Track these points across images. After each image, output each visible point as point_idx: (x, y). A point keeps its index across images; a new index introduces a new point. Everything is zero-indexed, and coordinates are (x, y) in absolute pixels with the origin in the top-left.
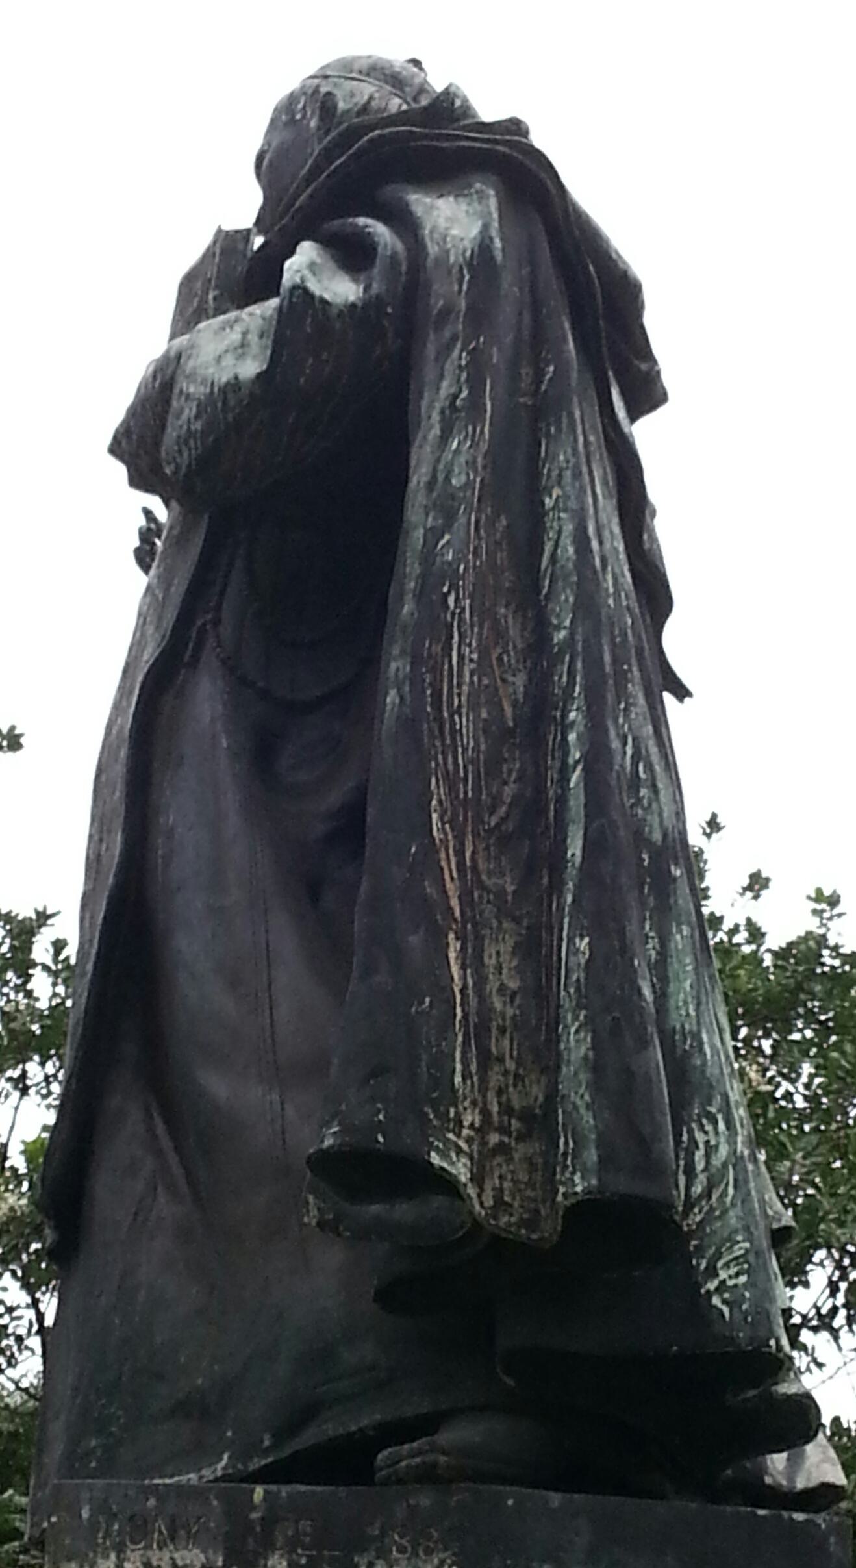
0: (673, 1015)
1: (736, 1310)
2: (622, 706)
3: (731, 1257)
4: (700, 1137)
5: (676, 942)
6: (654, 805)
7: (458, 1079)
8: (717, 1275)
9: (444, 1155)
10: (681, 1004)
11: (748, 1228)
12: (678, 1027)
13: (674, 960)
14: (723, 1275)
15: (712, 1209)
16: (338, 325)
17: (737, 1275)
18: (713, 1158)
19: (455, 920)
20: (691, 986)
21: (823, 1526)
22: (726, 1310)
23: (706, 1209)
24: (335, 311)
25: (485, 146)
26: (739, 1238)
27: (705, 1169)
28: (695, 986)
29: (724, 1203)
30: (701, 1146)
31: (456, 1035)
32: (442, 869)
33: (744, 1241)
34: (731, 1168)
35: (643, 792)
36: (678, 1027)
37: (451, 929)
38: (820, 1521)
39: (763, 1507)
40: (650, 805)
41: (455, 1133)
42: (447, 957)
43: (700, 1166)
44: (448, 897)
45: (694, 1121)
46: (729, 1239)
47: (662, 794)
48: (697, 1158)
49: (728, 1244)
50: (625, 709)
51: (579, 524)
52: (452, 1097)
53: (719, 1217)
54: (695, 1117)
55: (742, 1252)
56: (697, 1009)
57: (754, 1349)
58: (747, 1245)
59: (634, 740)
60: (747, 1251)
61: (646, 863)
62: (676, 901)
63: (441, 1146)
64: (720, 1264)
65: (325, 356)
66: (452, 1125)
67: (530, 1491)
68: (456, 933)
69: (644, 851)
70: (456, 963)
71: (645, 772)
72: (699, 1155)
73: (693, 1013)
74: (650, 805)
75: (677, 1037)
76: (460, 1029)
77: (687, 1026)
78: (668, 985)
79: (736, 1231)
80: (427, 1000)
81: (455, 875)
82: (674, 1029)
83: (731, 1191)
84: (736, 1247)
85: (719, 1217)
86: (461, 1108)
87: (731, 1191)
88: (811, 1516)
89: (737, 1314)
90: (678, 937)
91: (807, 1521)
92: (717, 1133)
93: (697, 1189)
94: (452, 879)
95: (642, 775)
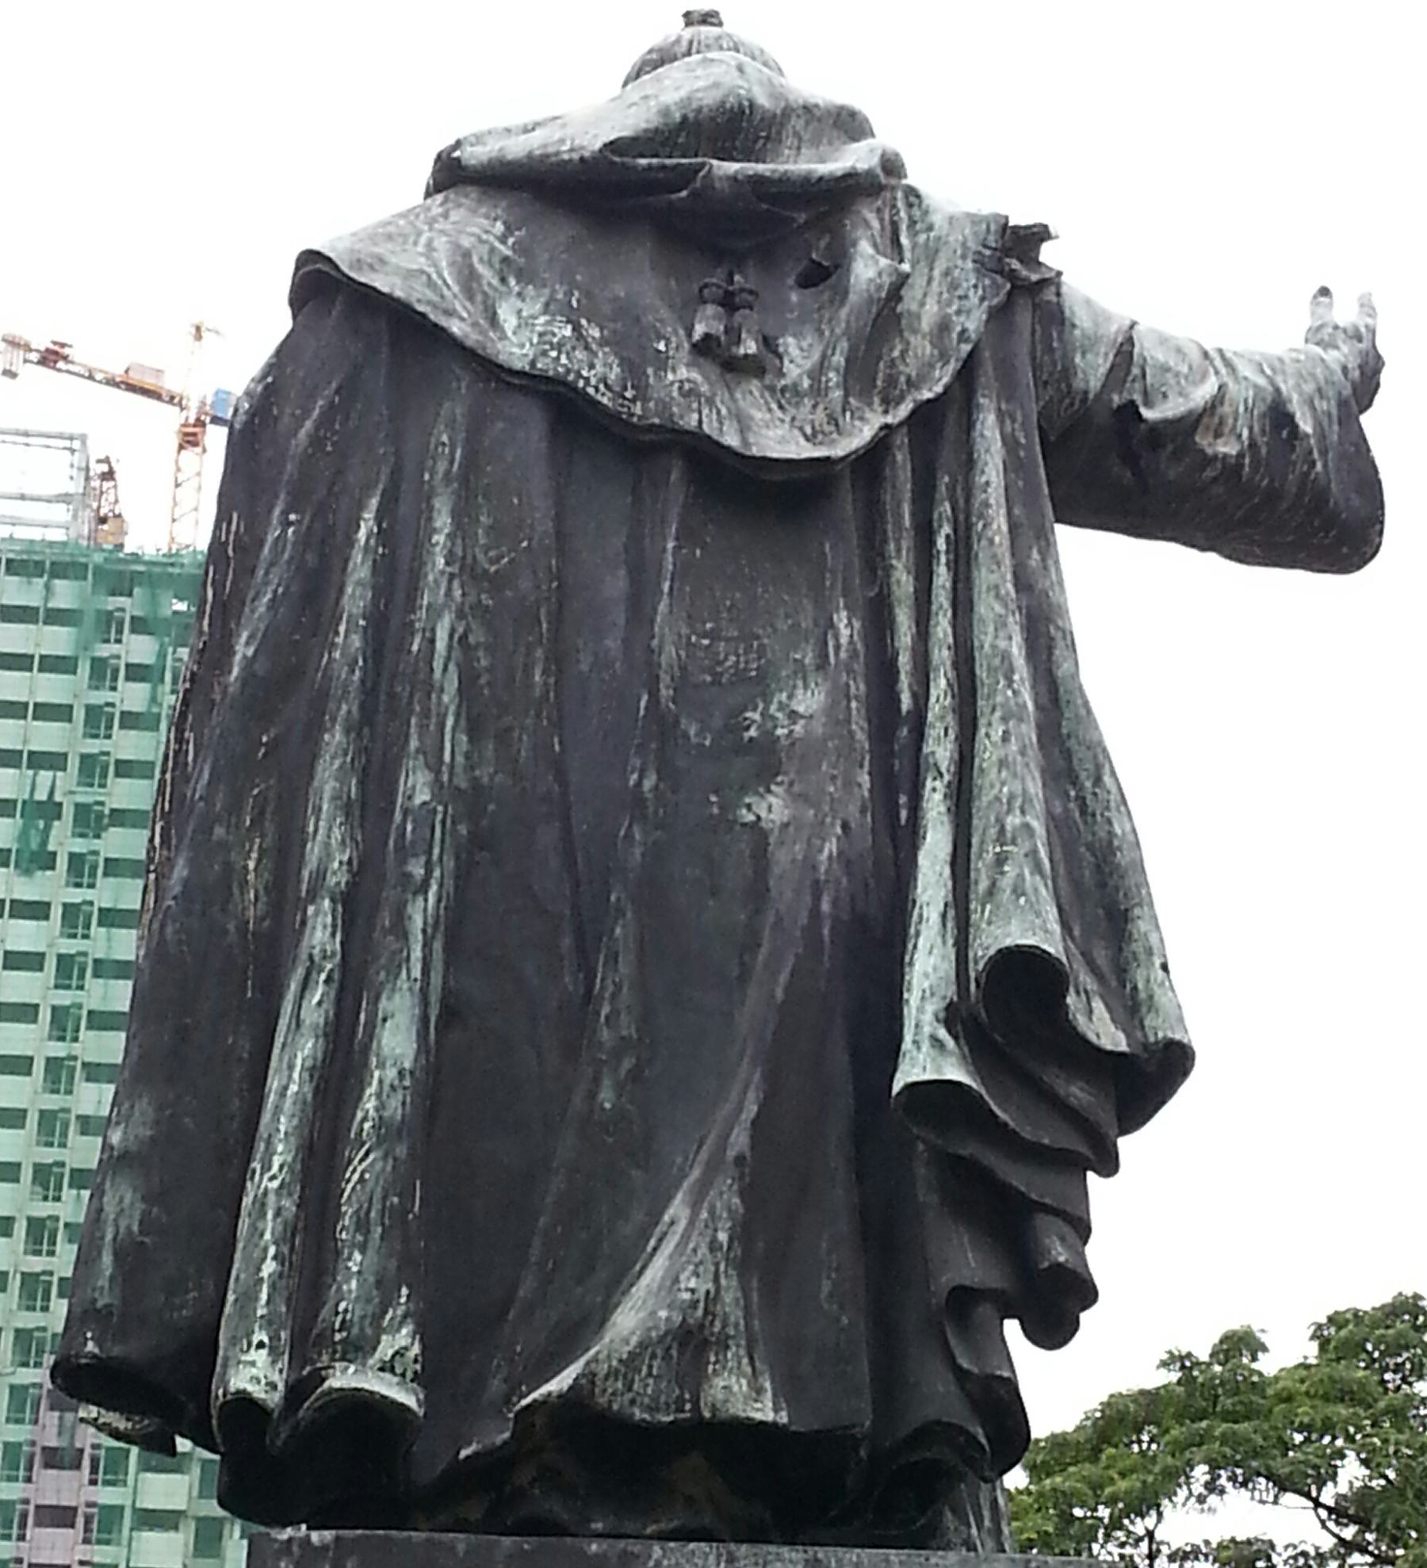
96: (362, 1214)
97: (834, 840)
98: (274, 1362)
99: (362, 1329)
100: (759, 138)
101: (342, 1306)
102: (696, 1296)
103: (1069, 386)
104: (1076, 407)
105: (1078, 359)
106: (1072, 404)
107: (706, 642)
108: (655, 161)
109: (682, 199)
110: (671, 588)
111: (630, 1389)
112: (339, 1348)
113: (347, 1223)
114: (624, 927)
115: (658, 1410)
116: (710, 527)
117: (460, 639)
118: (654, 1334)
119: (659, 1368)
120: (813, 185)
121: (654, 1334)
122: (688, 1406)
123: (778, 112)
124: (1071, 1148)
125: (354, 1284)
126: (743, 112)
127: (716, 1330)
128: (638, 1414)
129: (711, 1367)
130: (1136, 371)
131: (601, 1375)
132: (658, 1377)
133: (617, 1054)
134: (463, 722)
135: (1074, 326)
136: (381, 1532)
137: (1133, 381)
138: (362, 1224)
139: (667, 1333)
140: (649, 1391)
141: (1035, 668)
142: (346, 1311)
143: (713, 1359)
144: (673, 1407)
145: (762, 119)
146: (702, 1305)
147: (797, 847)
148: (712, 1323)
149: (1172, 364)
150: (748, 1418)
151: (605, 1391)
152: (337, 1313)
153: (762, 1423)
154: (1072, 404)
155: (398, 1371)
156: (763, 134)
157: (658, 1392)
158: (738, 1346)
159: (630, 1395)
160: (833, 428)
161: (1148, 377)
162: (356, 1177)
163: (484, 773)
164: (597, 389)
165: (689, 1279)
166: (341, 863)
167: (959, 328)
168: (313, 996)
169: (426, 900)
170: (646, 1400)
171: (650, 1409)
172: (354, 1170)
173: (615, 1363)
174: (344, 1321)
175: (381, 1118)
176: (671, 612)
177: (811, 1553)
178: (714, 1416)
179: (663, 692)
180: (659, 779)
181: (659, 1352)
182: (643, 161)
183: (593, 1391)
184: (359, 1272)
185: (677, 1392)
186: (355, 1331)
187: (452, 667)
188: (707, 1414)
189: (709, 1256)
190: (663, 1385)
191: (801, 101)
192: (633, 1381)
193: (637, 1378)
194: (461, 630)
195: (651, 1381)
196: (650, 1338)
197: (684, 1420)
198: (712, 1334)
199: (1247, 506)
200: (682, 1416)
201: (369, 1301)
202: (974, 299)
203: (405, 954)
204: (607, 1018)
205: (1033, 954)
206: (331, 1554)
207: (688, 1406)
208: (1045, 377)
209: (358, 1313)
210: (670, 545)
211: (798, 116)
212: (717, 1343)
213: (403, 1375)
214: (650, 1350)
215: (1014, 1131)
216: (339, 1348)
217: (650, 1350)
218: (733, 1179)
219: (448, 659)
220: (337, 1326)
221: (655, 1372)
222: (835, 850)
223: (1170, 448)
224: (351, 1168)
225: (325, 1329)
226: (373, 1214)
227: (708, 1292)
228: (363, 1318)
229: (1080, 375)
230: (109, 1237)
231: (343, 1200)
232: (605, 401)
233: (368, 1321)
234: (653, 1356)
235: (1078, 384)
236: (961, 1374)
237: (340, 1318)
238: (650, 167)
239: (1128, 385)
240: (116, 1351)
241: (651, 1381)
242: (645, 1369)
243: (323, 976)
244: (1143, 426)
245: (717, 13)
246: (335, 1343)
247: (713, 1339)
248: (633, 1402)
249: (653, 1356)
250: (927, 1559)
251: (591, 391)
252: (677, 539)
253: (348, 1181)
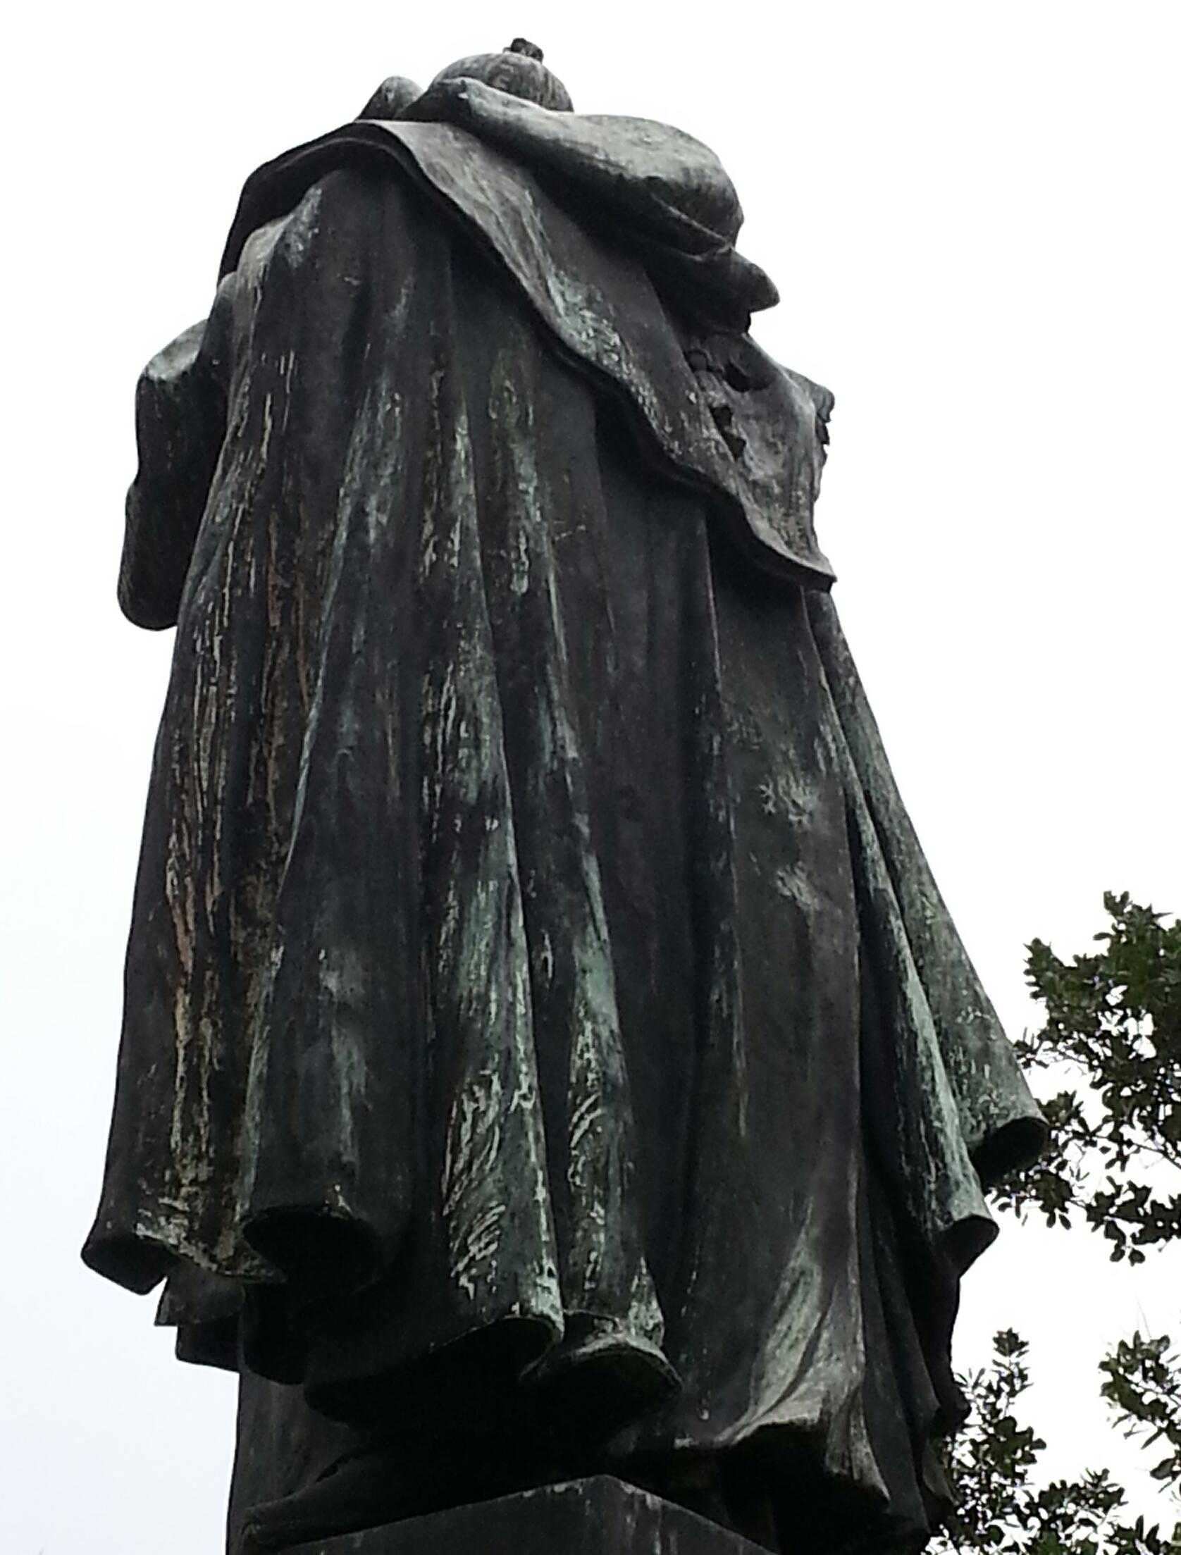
0: (463, 982)
1: (481, 1283)
2: (450, 669)
3: (482, 1228)
4: (469, 1107)
5: (479, 902)
6: (474, 764)
7: (176, 1138)
8: (468, 1251)
9: (150, 1223)
10: (472, 968)
11: (506, 1188)
12: (465, 994)
13: (472, 923)
14: (473, 1249)
15: (471, 1181)
16: (178, 400)
17: (488, 1245)
18: (480, 1124)
19: (186, 974)
20: (487, 945)
21: (581, 1491)
22: (471, 1287)
23: (466, 1182)
24: (171, 388)
25: (321, 146)
26: (493, 1204)
27: (471, 1140)
28: (491, 944)
29: (483, 1170)
30: (469, 1116)
31: (176, 1093)
32: (174, 926)
33: (498, 1206)
34: (497, 1130)
35: (463, 752)
36: (465, 994)
37: (180, 985)
38: (577, 1486)
39: (527, 1489)
40: (468, 764)
41: (169, 1196)
42: (174, 1015)
43: (466, 1137)
44: (178, 952)
45: (465, 1091)
46: (481, 1210)
47: (485, 751)
48: (463, 1132)
49: (480, 1215)
50: (453, 672)
51: (358, 503)
52: (169, 1158)
53: (476, 1188)
54: (466, 1087)
55: (495, 1218)
56: (489, 970)
57: (497, 1321)
58: (502, 1208)
59: (458, 699)
60: (501, 1215)
61: (458, 830)
62: (486, 857)
63: (149, 1214)
64: (470, 1240)
65: (179, 434)
66: (167, 1189)
67: (489, 1502)
68: (186, 987)
69: (458, 815)
70: (184, 1018)
71: (467, 731)
72: (466, 1127)
73: (483, 973)
74: (468, 764)
75: (463, 1006)
76: (181, 1086)
77: (475, 991)
78: (461, 953)
79: (490, 1198)
80: (153, 1067)
81: (191, 927)
82: (461, 996)
83: (493, 1154)
84: (488, 1216)
85: (476, 1188)
86: (178, 1167)
87: (493, 1154)
88: (570, 1484)
89: (482, 1288)
90: (482, 896)
91: (567, 1490)
92: (488, 1097)
93: (460, 1165)
94: (187, 931)
95: (463, 734)
96: (600, 1166)
99: (610, 1286)
101: (593, 1256)
109: (696, 263)
112: (587, 1296)
113: (580, 1168)
125: (602, 1237)
136: (691, 1513)
138: (598, 1175)
142: (596, 1262)
147: (835, 941)
152: (589, 1262)
160: (804, 545)
162: (585, 1125)
168: (517, 921)
172: (581, 1118)
174: (594, 1271)
175: (604, 1074)
184: (606, 1225)
186: (604, 1285)
188: (856, 1476)
199: (233, 670)
201: (616, 1259)
203: (587, 909)
206: (660, 1520)
209: (606, 1271)
215: (258, 1167)
216: (587, 1296)
220: (588, 1274)
224: (577, 1114)
225: (576, 1274)
226: (611, 1171)
228: (611, 1275)
230: (345, 1090)
231: (573, 1144)
233: (617, 1280)
236: (925, 1491)
237: (591, 1267)
238: (678, 220)
240: (364, 1215)
246: (584, 1290)
253: (576, 1126)
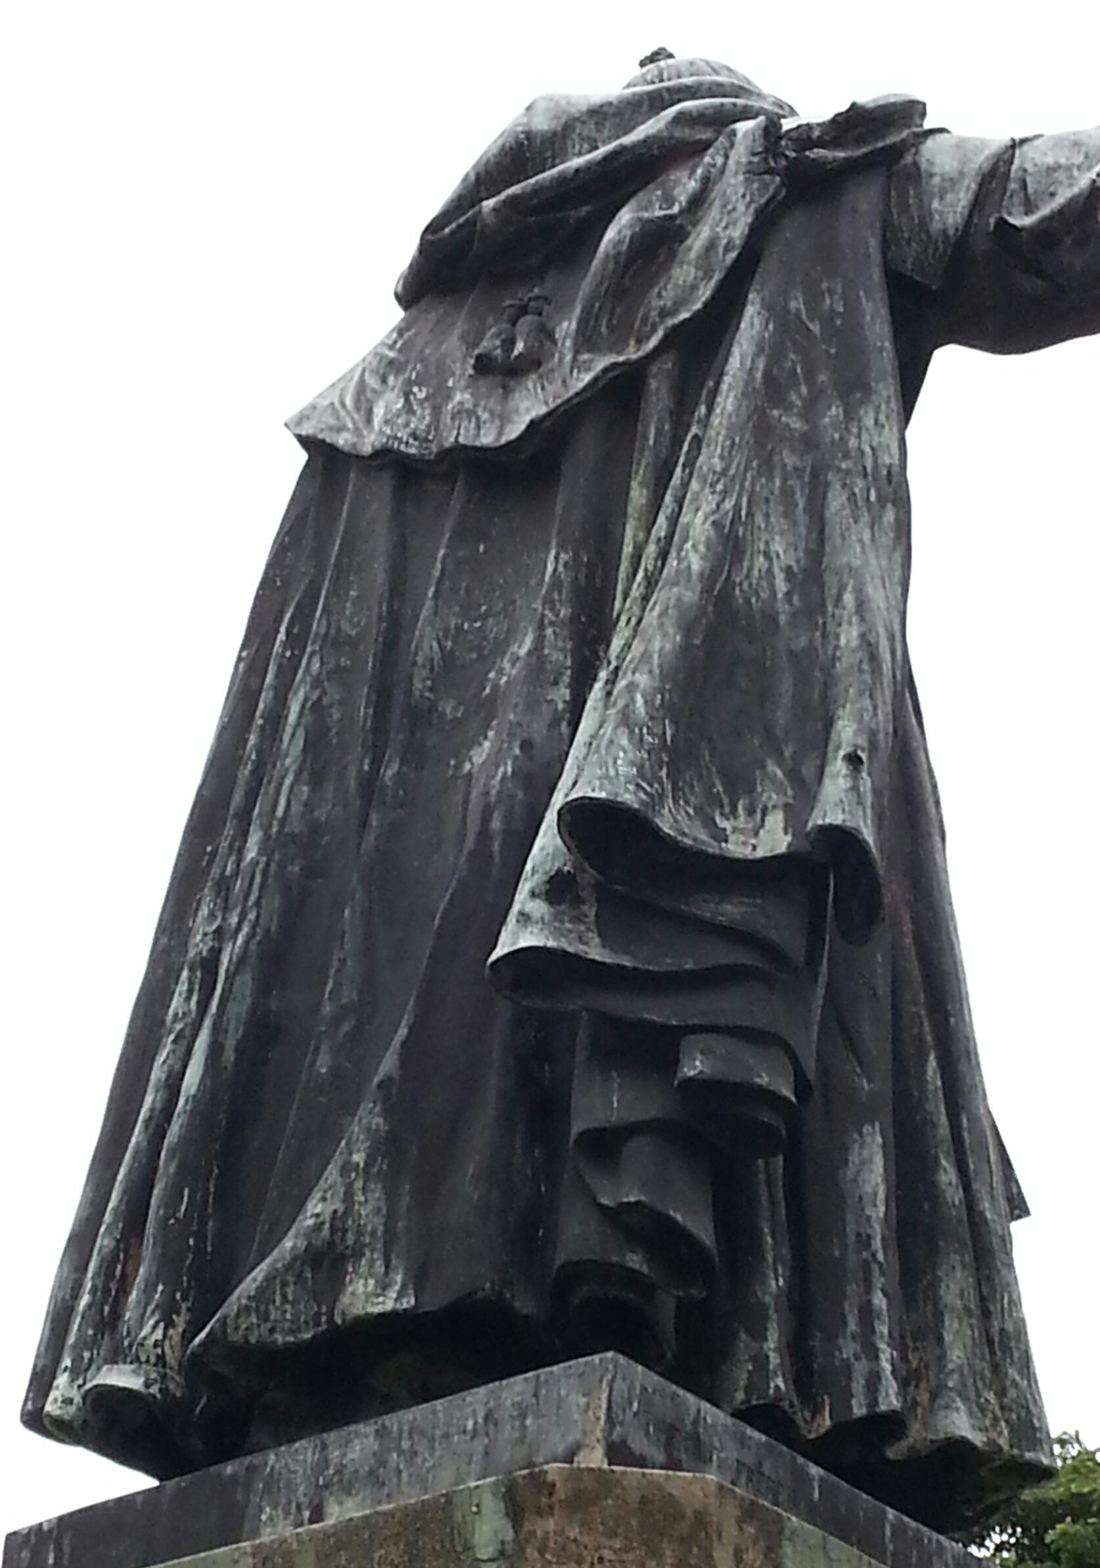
97: (509, 763)
98: (73, 1381)
100: (546, 159)
102: (321, 1219)
103: (928, 233)
104: (941, 247)
105: (936, 204)
106: (936, 249)
107: (478, 624)
108: (454, 225)
110: (436, 592)
111: (266, 1320)
114: (352, 908)
115: (299, 1330)
116: (496, 520)
117: (313, 705)
118: (279, 1265)
119: (294, 1293)
120: (572, 179)
121: (279, 1265)
122: (324, 1319)
123: (559, 129)
124: (710, 963)
126: (522, 144)
127: (350, 1243)
128: (279, 1338)
129: (348, 1278)
130: (1013, 186)
131: (233, 1314)
132: (294, 1303)
133: (336, 1022)
134: (305, 775)
135: (931, 175)
137: (1011, 196)
139: (295, 1259)
140: (288, 1316)
141: (811, 518)
143: (350, 1269)
144: (311, 1324)
145: (543, 142)
146: (327, 1226)
148: (343, 1239)
149: (1063, 161)
150: (367, 1314)
151: (237, 1329)
153: (382, 1315)
154: (936, 249)
155: (143, 1359)
156: (549, 154)
157: (296, 1316)
158: (372, 1251)
159: (269, 1325)
161: (1029, 185)
163: (321, 815)
164: (407, 443)
165: (315, 1206)
166: (205, 934)
167: (724, 242)
169: (234, 944)
170: (287, 1325)
171: (291, 1332)
173: (244, 1301)
176: (436, 614)
177: (380, 1422)
178: (344, 1321)
179: (418, 685)
180: (401, 764)
181: (290, 1279)
182: (447, 230)
183: (225, 1331)
185: (316, 1308)
187: (301, 733)
189: (339, 1179)
190: (302, 1307)
191: (584, 108)
192: (267, 1310)
193: (271, 1308)
194: (315, 697)
195: (288, 1307)
196: (277, 1270)
197: (323, 1332)
198: (347, 1247)
200: (320, 1329)
202: (741, 208)
204: (331, 992)
205: (584, 805)
207: (324, 1319)
208: (906, 235)
210: (441, 553)
211: (584, 123)
212: (353, 1256)
213: (147, 1361)
214: (278, 1281)
217: (278, 1281)
218: (375, 1102)
219: (298, 724)
220: (125, 1334)
221: (290, 1298)
222: (510, 770)
223: (1068, 241)
227: (335, 1212)
229: (937, 217)
232: (413, 451)
234: (284, 1284)
235: (936, 226)
238: (452, 233)
239: (1005, 203)
241: (288, 1307)
242: (278, 1299)
243: (172, 1037)
244: (1023, 234)
245: (664, 49)
247: (349, 1252)
248: (272, 1331)
249: (284, 1284)
250: (464, 1400)
251: (403, 447)
252: (447, 547)
